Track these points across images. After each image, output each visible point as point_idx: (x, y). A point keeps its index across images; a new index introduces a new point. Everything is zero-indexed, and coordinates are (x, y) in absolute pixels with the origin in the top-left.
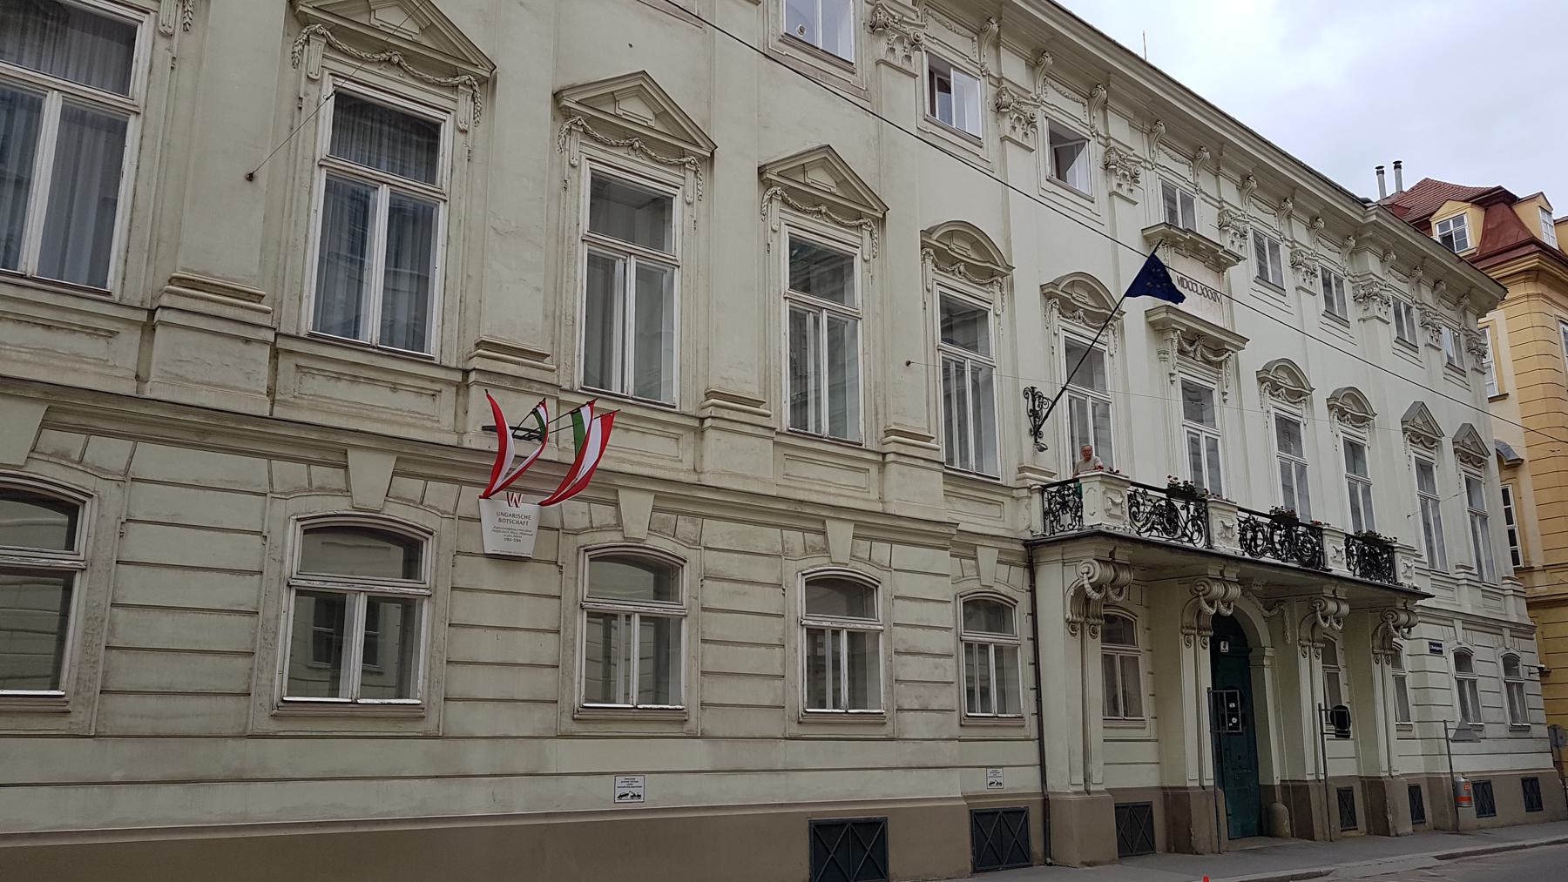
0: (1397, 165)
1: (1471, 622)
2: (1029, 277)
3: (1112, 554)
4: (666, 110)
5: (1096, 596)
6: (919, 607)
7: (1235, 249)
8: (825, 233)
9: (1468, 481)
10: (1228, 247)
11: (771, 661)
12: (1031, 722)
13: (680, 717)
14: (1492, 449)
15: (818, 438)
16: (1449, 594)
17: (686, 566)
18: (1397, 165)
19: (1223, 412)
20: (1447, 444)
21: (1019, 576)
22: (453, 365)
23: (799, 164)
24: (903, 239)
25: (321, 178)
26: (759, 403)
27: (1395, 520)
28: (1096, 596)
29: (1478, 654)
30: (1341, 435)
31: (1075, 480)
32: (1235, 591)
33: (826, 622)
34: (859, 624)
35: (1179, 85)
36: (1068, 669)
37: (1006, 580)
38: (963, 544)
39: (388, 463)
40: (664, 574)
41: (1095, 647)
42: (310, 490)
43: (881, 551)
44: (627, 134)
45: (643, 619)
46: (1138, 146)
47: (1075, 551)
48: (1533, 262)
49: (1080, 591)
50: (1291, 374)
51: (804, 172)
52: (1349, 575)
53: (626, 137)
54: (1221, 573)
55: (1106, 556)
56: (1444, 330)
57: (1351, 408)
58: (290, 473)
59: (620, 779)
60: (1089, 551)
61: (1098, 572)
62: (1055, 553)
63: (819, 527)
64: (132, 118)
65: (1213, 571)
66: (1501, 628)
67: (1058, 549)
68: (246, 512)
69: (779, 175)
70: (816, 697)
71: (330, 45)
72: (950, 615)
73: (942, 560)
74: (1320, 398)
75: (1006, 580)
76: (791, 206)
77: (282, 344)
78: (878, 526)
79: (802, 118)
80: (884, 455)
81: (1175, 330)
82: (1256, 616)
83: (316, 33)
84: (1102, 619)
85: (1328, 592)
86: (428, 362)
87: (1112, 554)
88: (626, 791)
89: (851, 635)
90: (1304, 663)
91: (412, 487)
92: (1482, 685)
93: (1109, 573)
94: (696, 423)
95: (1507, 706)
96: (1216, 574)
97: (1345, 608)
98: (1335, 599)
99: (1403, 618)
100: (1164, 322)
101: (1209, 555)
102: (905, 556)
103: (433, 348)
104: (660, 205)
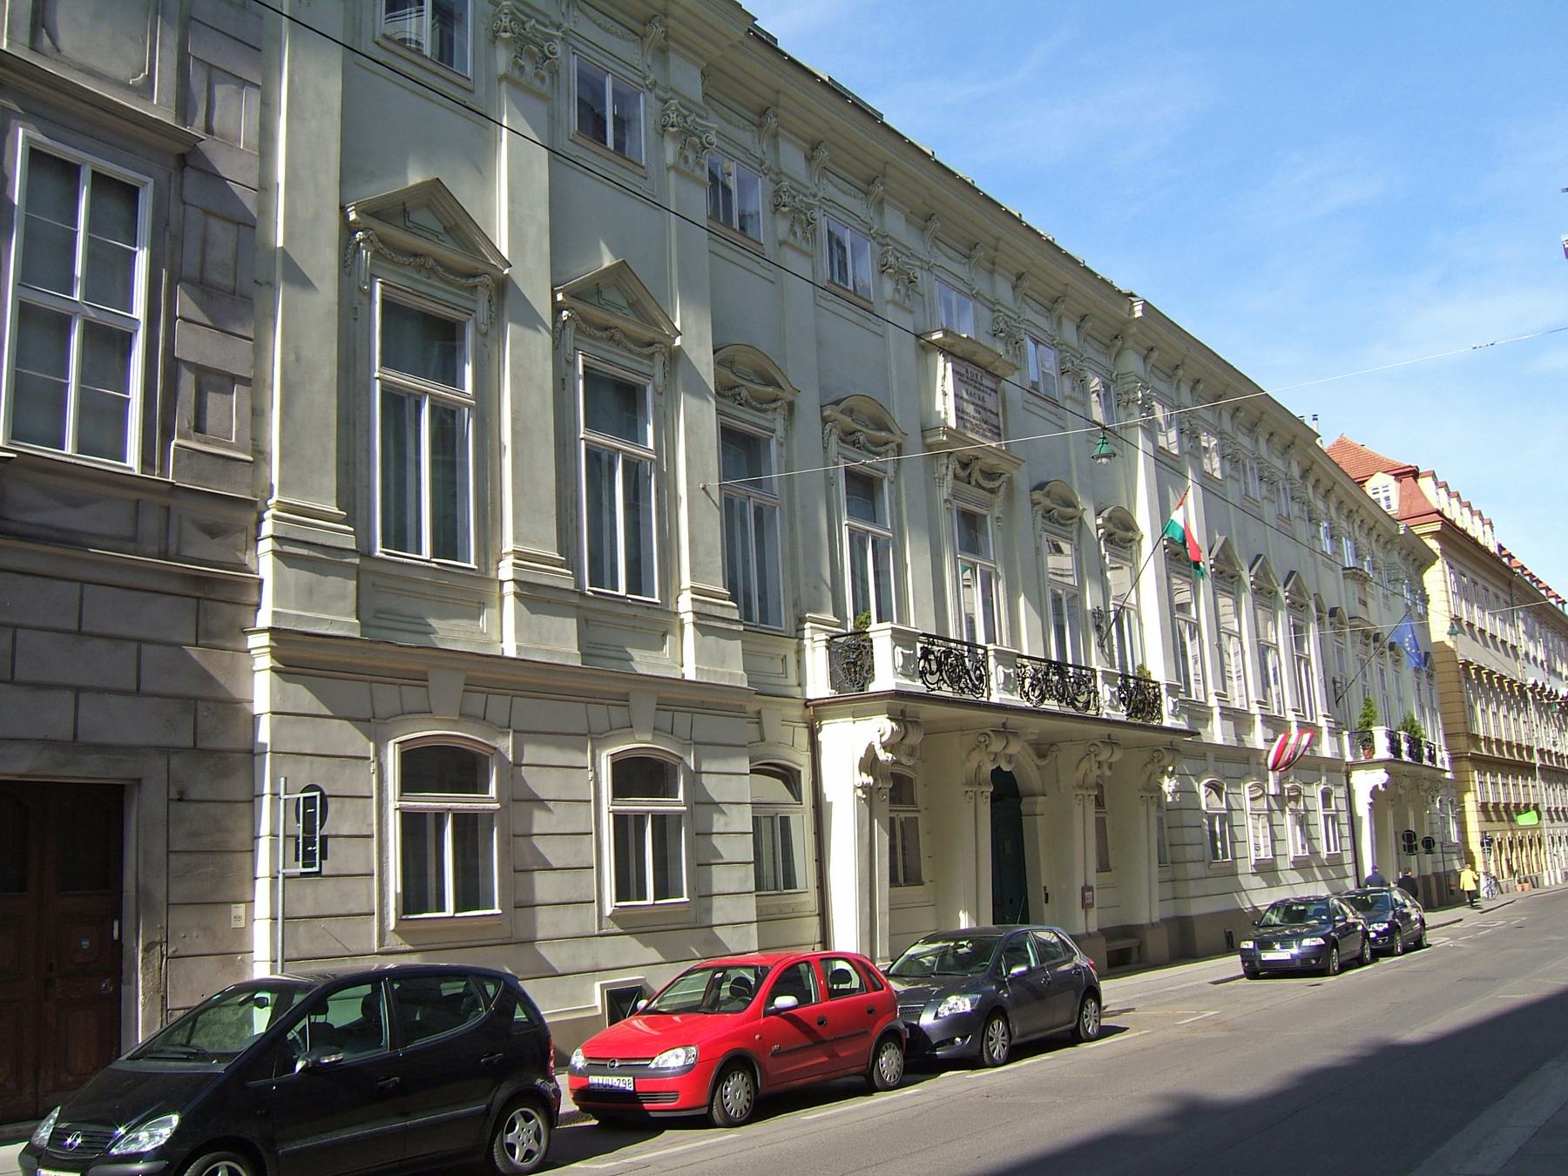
5: (883, 756)
48: (1437, 527)
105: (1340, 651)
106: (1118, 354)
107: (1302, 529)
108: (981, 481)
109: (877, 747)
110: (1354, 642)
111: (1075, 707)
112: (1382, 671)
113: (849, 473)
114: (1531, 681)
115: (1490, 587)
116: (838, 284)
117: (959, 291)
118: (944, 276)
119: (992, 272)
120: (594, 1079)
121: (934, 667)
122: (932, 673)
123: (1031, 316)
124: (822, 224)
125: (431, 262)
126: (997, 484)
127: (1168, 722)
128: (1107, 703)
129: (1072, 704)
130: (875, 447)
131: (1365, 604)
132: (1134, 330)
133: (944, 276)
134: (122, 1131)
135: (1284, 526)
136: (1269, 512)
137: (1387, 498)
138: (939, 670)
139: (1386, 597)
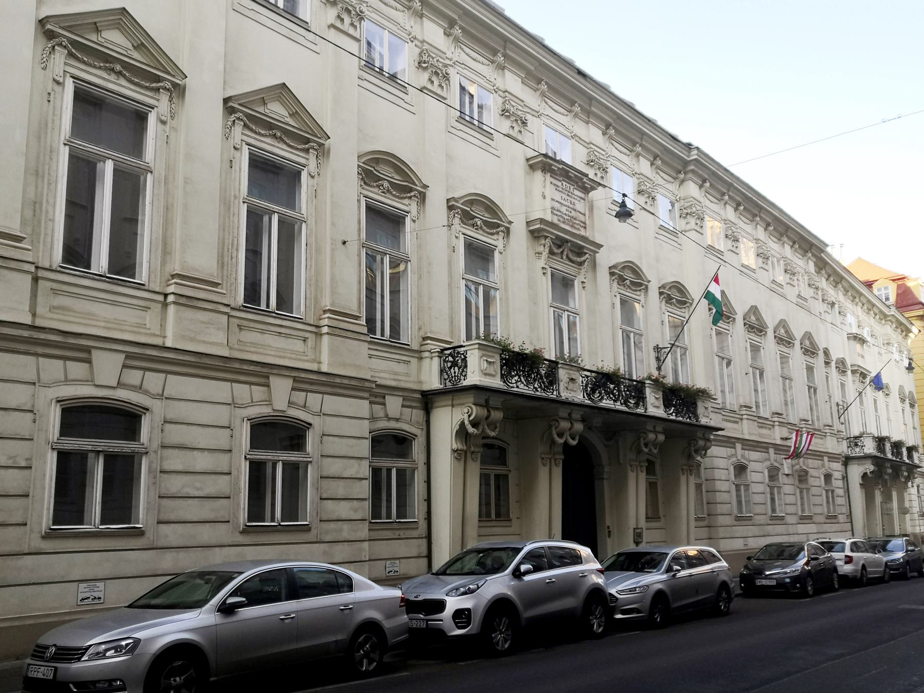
2: (606, 259)
5: (471, 430)
6: (340, 438)
7: (598, 179)
10: (591, 176)
11: (220, 485)
12: (423, 524)
14: (821, 349)
15: (267, 313)
16: (735, 426)
17: (311, 430)
19: (579, 298)
20: (797, 343)
21: (418, 415)
22: (157, 290)
25: (244, 208)
26: (216, 285)
27: (695, 373)
29: (752, 466)
32: (579, 427)
39: (288, 383)
40: (126, 420)
41: (475, 469)
42: (67, 381)
43: (314, 400)
45: (284, 464)
46: (531, 98)
49: (462, 424)
51: (265, 104)
52: (664, 415)
54: (654, 427)
55: (483, 402)
56: (659, 197)
59: (82, 586)
64: (149, 174)
66: (823, 456)
69: (239, 104)
71: (245, 126)
72: (365, 448)
73: (362, 407)
77: (41, 273)
78: (308, 380)
80: (166, 295)
81: (546, 237)
83: (238, 119)
85: (649, 427)
86: (140, 286)
88: (88, 595)
89: (285, 464)
90: (632, 476)
92: (754, 488)
93: (484, 412)
94: (161, 298)
95: (799, 503)
97: (661, 438)
98: (656, 432)
102: (333, 403)
103: (143, 276)
105: (843, 385)
108: (571, 256)
109: (466, 422)
111: (627, 406)
116: (469, 120)
119: (421, 18)
125: (386, 184)
126: (583, 259)
131: (863, 357)
134: (788, 580)
135: (775, 287)
136: (791, 293)
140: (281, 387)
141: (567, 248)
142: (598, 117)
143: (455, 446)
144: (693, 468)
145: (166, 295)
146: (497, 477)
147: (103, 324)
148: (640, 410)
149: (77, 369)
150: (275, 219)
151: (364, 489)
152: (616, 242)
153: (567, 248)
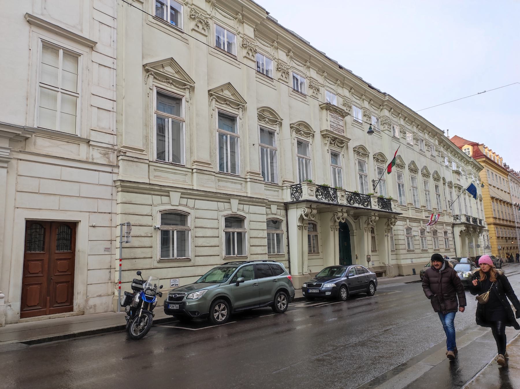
0: (448, 130)
1: (412, 220)
3: (311, 206)
4: (180, 70)
5: (305, 218)
8: (229, 110)
9: (359, 162)
13: (189, 260)
18: (448, 130)
19: (341, 160)
21: (283, 212)
23: (162, 64)
24: (252, 112)
26: (210, 164)
28: (305, 218)
30: (296, 139)
31: (300, 184)
32: (345, 215)
33: (230, 230)
34: (278, 232)
35: (315, 49)
36: (296, 239)
37: (280, 214)
38: (267, 203)
44: (167, 78)
46: (320, 79)
47: (300, 205)
48: (484, 159)
49: (301, 216)
50: (382, 156)
51: (223, 91)
52: (379, 209)
53: (167, 79)
55: (309, 206)
57: (302, 129)
58: (157, 199)
59: (172, 280)
60: (304, 205)
61: (307, 210)
62: (295, 206)
63: (228, 201)
65: (339, 209)
66: (168, 192)
67: (296, 204)
68: (214, 215)
70: (228, 252)
73: (263, 210)
74: (286, 124)
75: (280, 214)
76: (218, 102)
79: (225, 72)
82: (351, 220)
84: (309, 225)
87: (311, 206)
90: (366, 234)
91: (184, 201)
93: (310, 211)
94: (191, 170)
96: (340, 210)
97: (377, 218)
98: (375, 216)
99: (393, 220)
100: (326, 134)
101: (337, 205)
104: (177, 100)
106: (381, 110)
107: (440, 159)
108: (338, 144)
109: (303, 215)
110: (455, 191)
112: (465, 199)
113: (378, 168)
114: (515, 203)
115: (502, 177)
117: (333, 93)
118: (328, 89)
120: (310, 291)
121: (320, 193)
122: (320, 195)
123: (354, 100)
124: (291, 74)
127: (374, 207)
128: (375, 205)
129: (363, 205)
130: (308, 134)
131: (459, 180)
132: (386, 103)
133: (328, 89)
137: (469, 152)
138: (322, 194)
139: (466, 179)
140: (235, 202)
141: (337, 141)
142: (284, 47)
143: (298, 224)
144: (390, 230)
145: (192, 169)
146: (238, 233)
147: (172, 182)
148: (369, 207)
149: (165, 199)
150: (170, 120)
151: (265, 242)
152: (357, 136)
153: (337, 141)
